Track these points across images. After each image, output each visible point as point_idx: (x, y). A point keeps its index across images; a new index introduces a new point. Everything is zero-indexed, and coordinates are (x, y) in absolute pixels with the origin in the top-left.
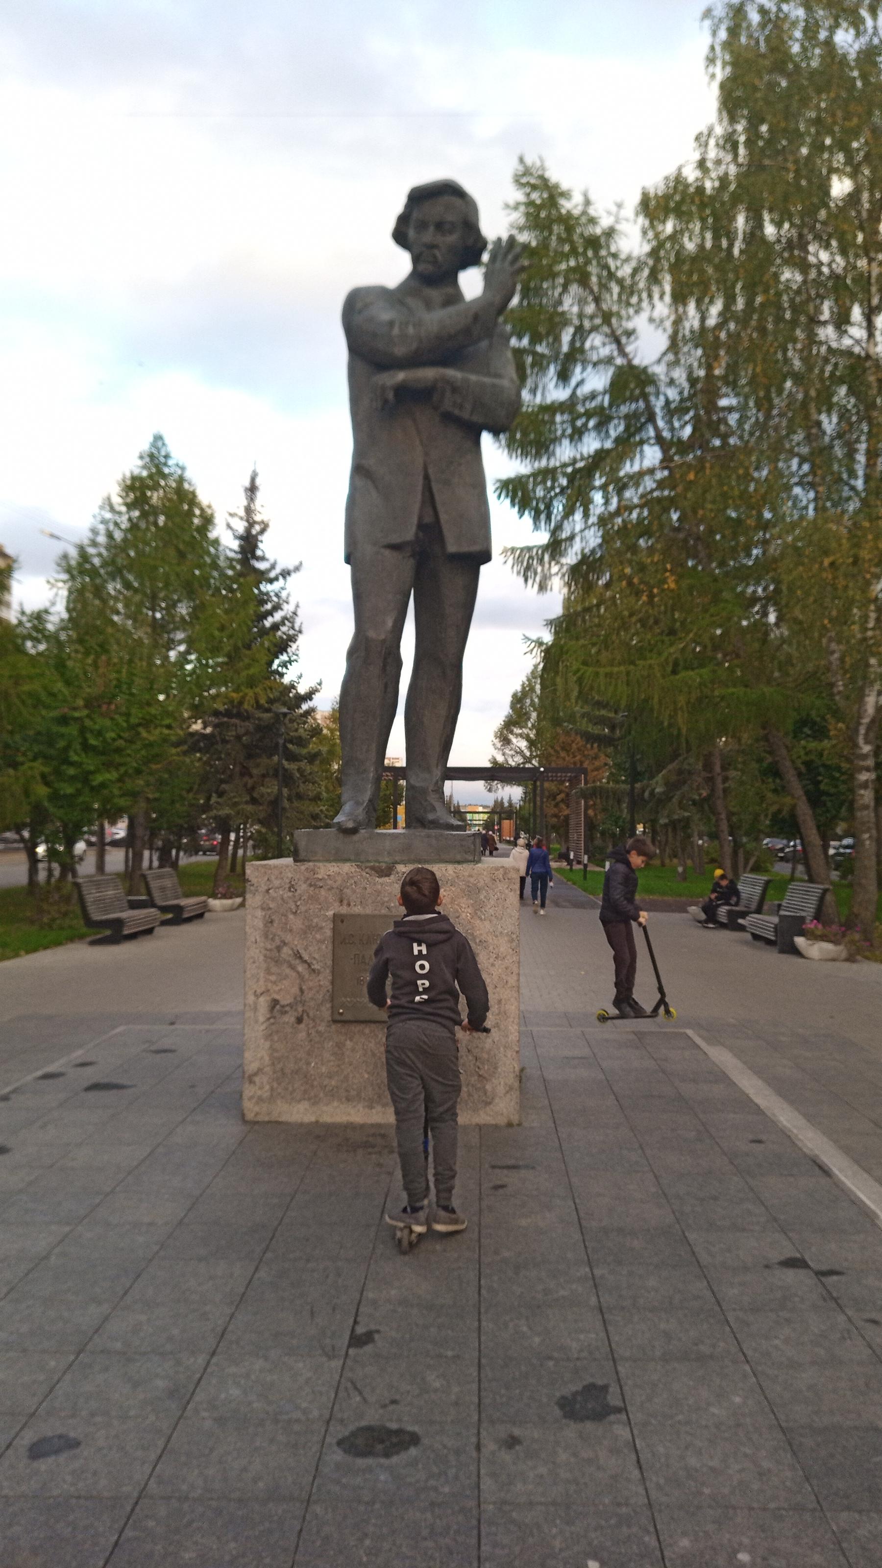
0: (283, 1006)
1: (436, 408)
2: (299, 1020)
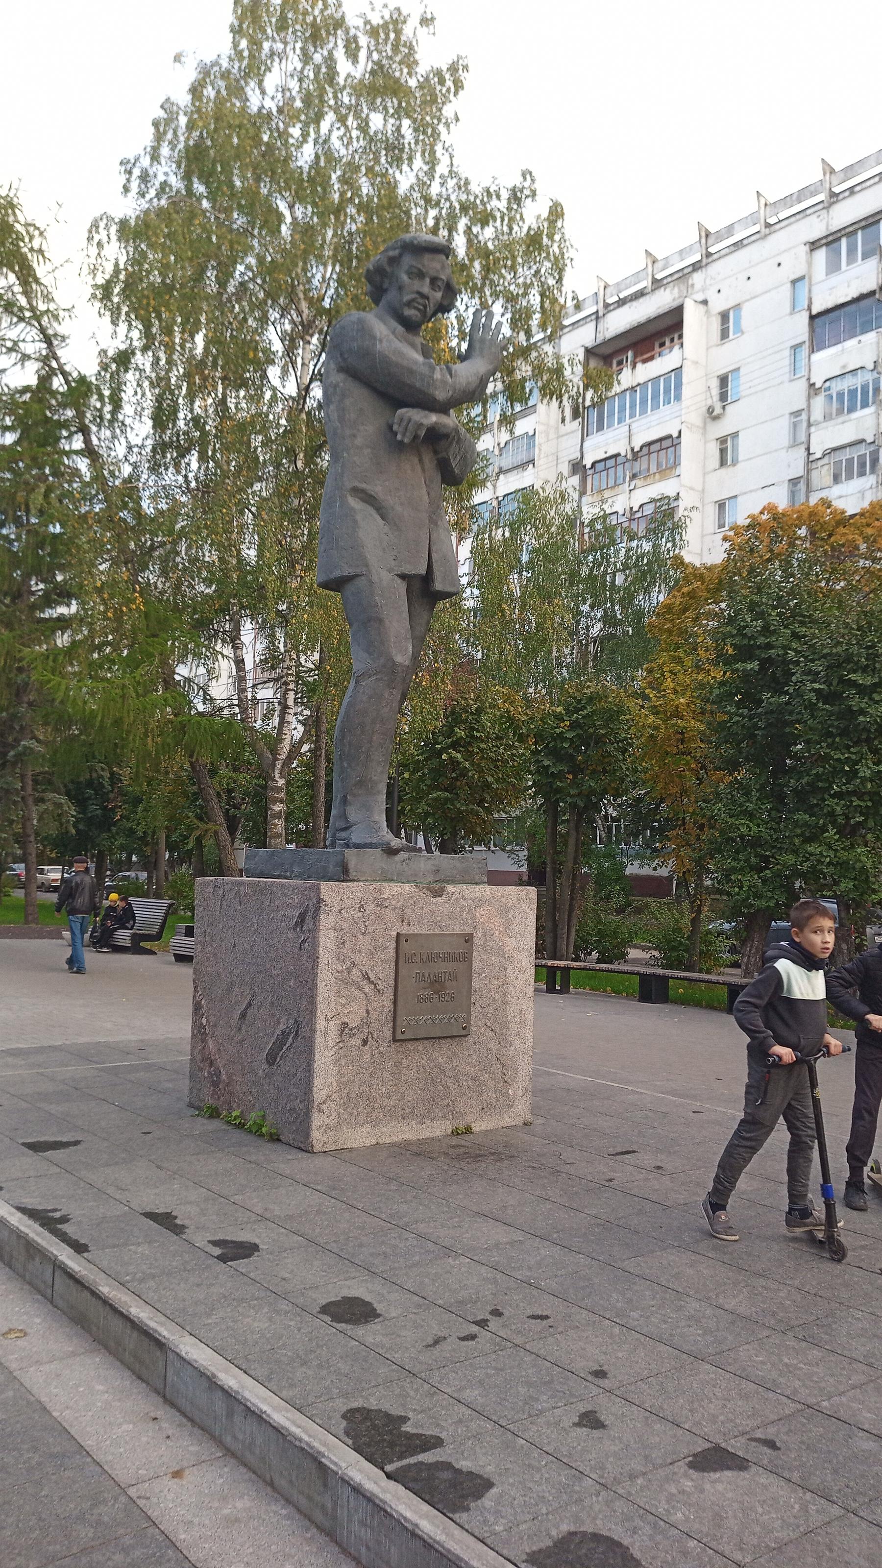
0: (351, 1030)
1: (436, 452)
2: (365, 1042)
